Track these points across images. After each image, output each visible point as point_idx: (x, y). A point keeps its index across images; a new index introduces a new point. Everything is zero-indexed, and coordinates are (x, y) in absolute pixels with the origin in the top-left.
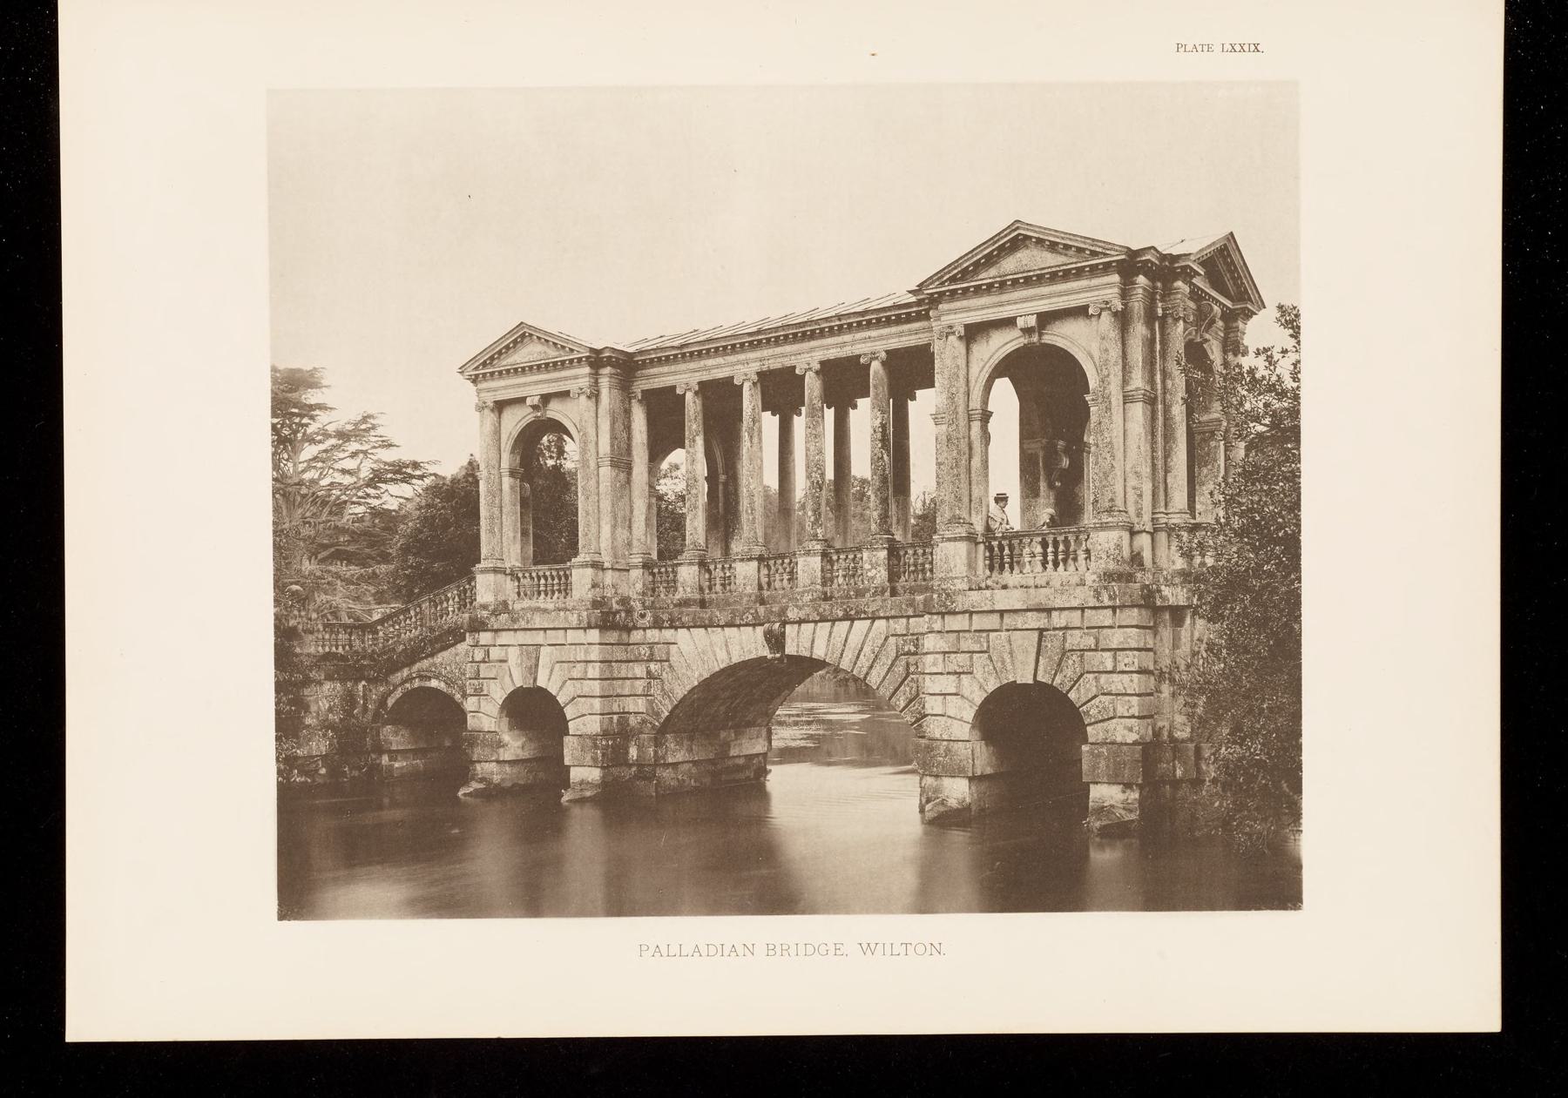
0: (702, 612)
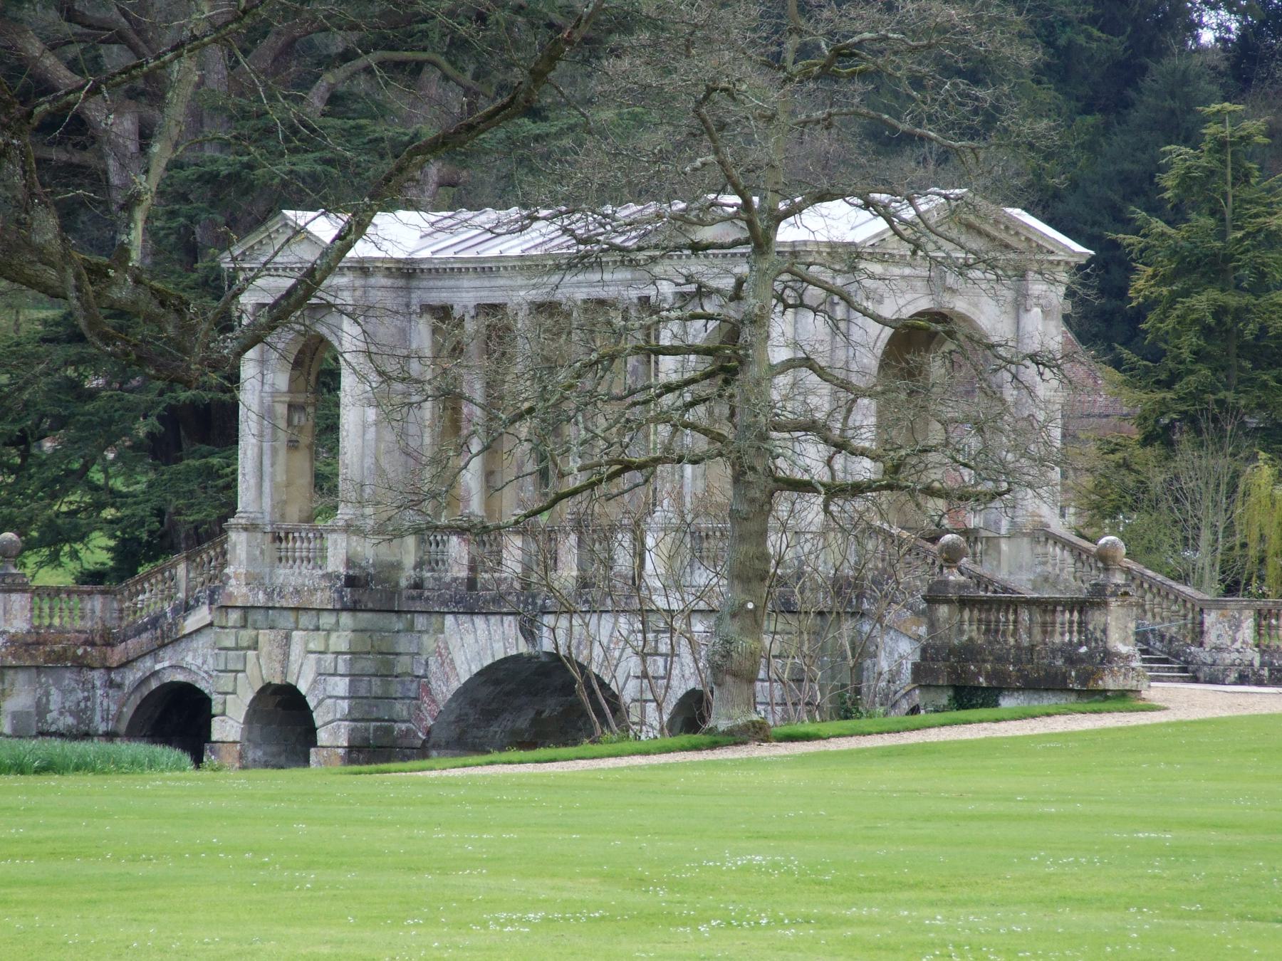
0: (471, 600)
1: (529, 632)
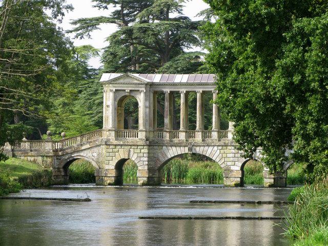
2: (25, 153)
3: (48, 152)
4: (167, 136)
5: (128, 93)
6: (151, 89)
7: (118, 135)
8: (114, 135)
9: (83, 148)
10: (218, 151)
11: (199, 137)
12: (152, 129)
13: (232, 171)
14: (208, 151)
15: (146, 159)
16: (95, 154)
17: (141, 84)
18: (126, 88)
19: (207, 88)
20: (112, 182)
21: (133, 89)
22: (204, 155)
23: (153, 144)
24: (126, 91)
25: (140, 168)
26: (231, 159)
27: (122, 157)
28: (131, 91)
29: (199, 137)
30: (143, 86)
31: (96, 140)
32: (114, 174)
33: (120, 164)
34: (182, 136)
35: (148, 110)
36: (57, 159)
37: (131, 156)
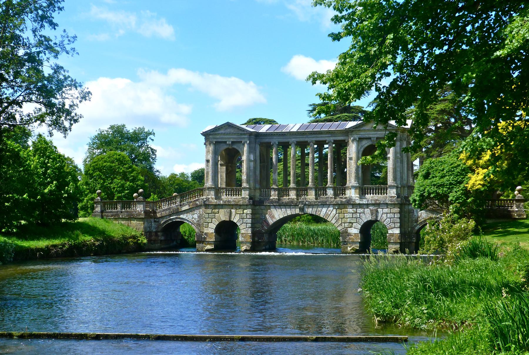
0: (280, 205)
1: (302, 209)
2: (116, 217)
3: (139, 214)
4: (274, 196)
5: (229, 145)
6: (257, 140)
7: (363, 192)
8: (213, 194)
9: (184, 208)
10: (335, 210)
11: (311, 196)
12: (258, 186)
13: (349, 235)
14: (322, 212)
15: (249, 221)
16: (196, 216)
17: (244, 134)
18: (371, 136)
19: (322, 137)
20: (248, 248)
21: (235, 140)
22: (324, 219)
23: (258, 204)
24: (228, 143)
25: (243, 231)
26: (348, 220)
27: (370, 219)
28: (233, 143)
29: (311, 196)
30: (246, 136)
31: (197, 200)
32: (213, 239)
33: (367, 228)
34: (293, 195)
35: (252, 164)
36: (155, 221)
37: (233, 217)
